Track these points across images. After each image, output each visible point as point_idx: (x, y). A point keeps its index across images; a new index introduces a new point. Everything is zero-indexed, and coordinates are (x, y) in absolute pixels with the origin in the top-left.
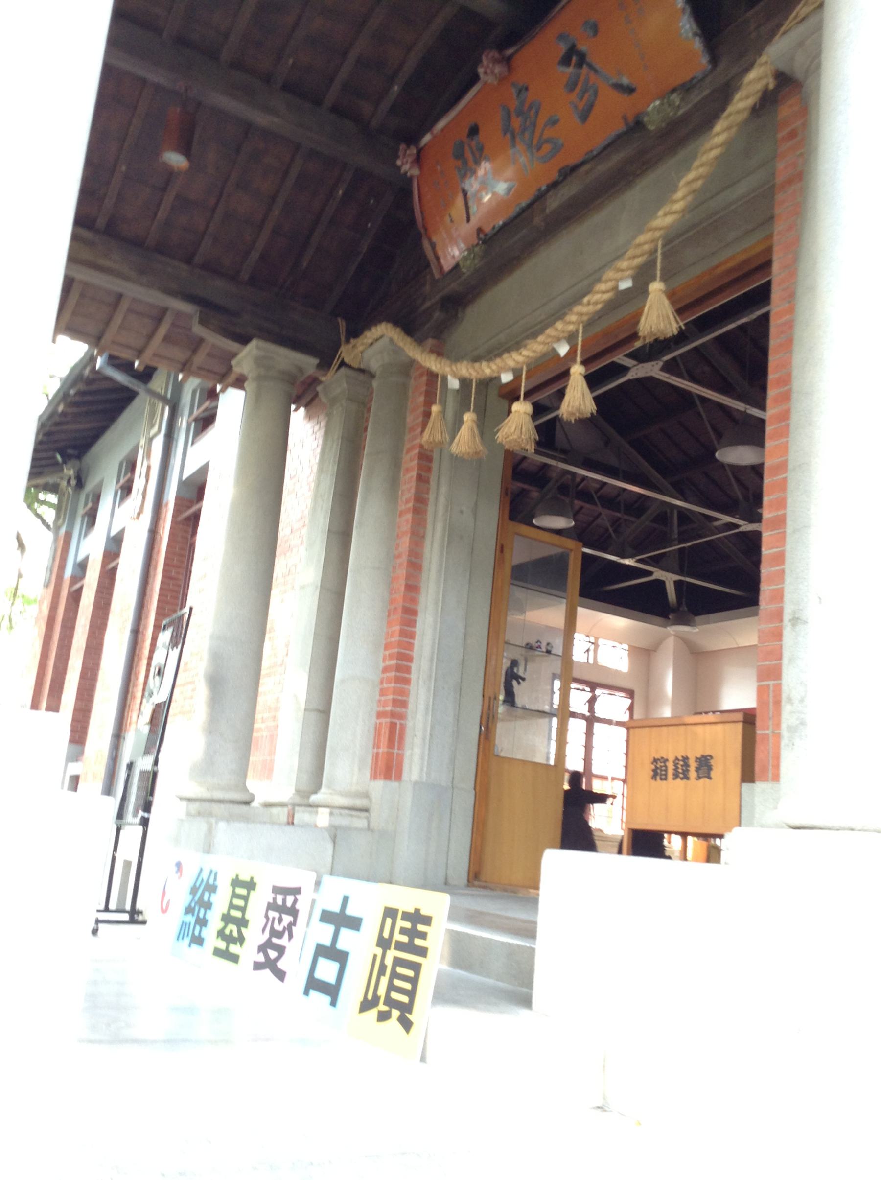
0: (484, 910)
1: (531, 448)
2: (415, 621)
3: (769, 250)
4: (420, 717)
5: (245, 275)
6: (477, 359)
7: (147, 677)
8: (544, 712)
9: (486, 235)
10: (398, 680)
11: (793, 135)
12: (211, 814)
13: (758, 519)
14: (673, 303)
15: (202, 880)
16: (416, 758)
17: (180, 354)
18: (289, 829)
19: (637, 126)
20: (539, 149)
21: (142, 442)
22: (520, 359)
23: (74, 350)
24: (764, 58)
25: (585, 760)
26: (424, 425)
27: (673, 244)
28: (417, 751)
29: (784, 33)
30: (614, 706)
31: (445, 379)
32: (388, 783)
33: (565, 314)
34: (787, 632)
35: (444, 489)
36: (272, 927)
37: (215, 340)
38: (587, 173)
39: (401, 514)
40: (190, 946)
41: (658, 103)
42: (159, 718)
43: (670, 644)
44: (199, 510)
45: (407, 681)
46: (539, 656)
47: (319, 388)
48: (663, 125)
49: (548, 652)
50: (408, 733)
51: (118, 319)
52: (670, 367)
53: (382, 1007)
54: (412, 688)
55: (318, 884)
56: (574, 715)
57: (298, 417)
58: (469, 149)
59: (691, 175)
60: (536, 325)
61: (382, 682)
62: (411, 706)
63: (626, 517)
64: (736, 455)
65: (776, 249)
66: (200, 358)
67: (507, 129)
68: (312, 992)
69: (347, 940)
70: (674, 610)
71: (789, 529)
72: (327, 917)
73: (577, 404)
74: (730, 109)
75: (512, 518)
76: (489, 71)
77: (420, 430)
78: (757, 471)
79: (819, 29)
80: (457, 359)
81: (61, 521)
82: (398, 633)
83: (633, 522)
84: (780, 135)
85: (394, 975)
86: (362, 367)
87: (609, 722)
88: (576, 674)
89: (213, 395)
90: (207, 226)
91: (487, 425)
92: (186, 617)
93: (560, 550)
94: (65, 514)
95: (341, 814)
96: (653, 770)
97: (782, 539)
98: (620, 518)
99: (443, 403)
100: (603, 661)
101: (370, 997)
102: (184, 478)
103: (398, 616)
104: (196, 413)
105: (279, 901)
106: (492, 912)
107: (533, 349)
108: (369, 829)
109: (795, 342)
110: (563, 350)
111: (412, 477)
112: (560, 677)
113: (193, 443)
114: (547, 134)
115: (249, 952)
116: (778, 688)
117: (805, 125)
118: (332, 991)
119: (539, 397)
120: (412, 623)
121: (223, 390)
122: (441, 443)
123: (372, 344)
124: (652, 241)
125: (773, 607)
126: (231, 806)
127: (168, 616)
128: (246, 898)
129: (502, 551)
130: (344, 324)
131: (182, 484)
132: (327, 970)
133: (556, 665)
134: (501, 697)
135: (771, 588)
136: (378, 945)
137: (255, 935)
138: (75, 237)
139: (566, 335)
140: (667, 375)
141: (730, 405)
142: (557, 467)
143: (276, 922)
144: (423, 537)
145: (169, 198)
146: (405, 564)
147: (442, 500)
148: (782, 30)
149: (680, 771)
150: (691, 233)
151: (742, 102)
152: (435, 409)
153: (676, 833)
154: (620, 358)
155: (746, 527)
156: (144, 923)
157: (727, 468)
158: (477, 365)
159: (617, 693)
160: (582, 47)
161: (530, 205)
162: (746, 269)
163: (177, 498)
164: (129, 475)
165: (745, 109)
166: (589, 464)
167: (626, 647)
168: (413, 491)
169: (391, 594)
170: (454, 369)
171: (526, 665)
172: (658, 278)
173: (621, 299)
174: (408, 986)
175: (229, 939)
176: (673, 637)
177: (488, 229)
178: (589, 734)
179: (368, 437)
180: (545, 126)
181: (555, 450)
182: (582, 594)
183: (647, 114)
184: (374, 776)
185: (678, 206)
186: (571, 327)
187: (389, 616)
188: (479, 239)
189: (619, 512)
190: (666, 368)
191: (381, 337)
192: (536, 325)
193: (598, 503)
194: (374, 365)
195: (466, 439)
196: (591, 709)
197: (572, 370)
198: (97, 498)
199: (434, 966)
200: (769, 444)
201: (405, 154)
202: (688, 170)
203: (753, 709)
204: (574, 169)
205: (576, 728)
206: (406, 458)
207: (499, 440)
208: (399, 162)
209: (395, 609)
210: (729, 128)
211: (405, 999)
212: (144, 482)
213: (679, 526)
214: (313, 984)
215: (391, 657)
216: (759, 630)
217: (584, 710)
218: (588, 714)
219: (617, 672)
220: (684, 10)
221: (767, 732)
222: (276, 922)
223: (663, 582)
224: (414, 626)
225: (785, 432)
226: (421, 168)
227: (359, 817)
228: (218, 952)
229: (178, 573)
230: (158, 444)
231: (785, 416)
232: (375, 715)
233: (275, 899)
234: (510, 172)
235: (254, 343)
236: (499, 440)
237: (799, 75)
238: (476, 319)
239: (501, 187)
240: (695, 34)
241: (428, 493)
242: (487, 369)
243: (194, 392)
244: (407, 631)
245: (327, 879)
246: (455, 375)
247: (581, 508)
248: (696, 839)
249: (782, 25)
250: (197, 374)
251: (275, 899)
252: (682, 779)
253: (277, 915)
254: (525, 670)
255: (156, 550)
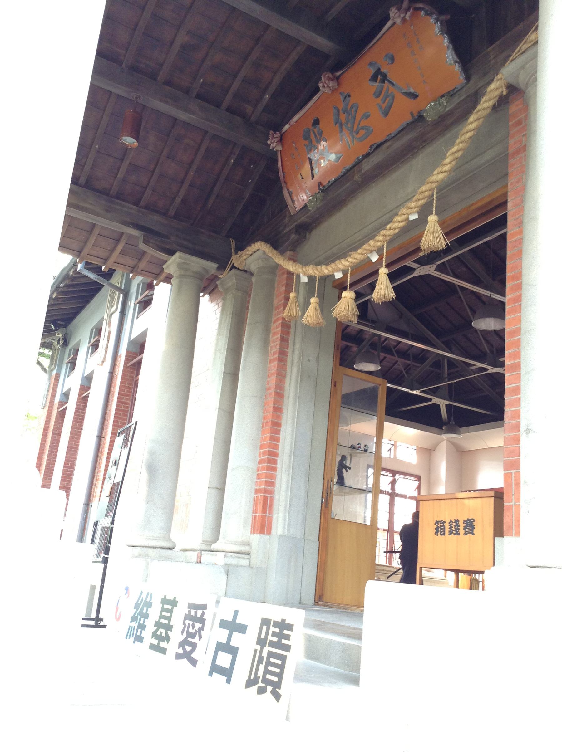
0: (326, 620)
1: (355, 320)
2: (280, 431)
3: (505, 194)
4: (283, 492)
5: (172, 212)
6: (318, 264)
7: (107, 466)
8: (363, 490)
9: (324, 187)
10: (269, 469)
11: (519, 123)
12: (147, 556)
13: (502, 365)
14: (442, 229)
15: (142, 600)
16: (281, 520)
17: (131, 262)
18: (199, 565)
19: (420, 118)
20: (357, 133)
21: (106, 316)
22: (347, 264)
23: (66, 259)
24: (499, 76)
25: (389, 521)
26: (285, 306)
27: (442, 192)
28: (281, 515)
29: (512, 61)
30: (407, 486)
31: (298, 277)
32: (262, 535)
33: (375, 236)
34: (524, 439)
35: (298, 346)
36: (188, 632)
37: (153, 253)
38: (388, 148)
39: (271, 362)
40: (134, 642)
41: (433, 104)
42: (115, 492)
43: (444, 446)
44: (141, 359)
45: (275, 469)
46: (360, 453)
47: (218, 282)
48: (436, 117)
49: (366, 451)
50: (276, 503)
51: (92, 240)
52: (440, 269)
53: (260, 684)
54: (278, 474)
55: (218, 602)
56: (382, 492)
57: (205, 300)
58: (313, 134)
59: (455, 149)
60: (355, 243)
61: (258, 470)
62: (277, 485)
63: (413, 363)
64: (486, 324)
65: (509, 194)
66: (143, 265)
67: (337, 121)
68: (214, 674)
69: (237, 640)
70: (446, 424)
71: (523, 372)
72: (224, 624)
73: (383, 293)
74: (479, 107)
75: (341, 365)
76: (325, 86)
77: (282, 308)
78: (500, 335)
79: (535, 57)
80: (305, 264)
81: (53, 366)
82: (268, 438)
83: (418, 367)
84: (511, 123)
85: (269, 663)
86: (245, 269)
87: (405, 497)
88: (384, 465)
89: (151, 287)
90: (148, 183)
91: (326, 306)
92: (133, 428)
93: (373, 385)
94: (56, 363)
95: (231, 556)
96: (436, 529)
97: (518, 377)
98: (409, 365)
99: (297, 292)
100: (399, 457)
101: (252, 677)
102: (132, 337)
103: (268, 427)
104: (140, 298)
105: (193, 613)
106: (330, 622)
107: (355, 257)
108: (250, 566)
109: (524, 252)
110: (374, 258)
111: (277, 338)
112: (373, 467)
113: (137, 318)
114: (362, 124)
115: (173, 647)
116: (518, 475)
117: (527, 117)
118: (227, 673)
119: (358, 287)
120: (278, 432)
121: (157, 284)
122: (296, 317)
123: (251, 255)
124: (430, 190)
125: (513, 422)
126: (160, 550)
127: (122, 427)
128: (171, 611)
129: (335, 386)
130: (234, 242)
131: (131, 343)
132: (224, 660)
133: (371, 460)
134: (335, 480)
135: (511, 409)
136: (257, 643)
137: (177, 636)
138: (71, 191)
139: (376, 248)
140: (439, 273)
141: (480, 292)
142: (369, 332)
143: (191, 627)
144: (285, 376)
145: (125, 166)
146: (273, 394)
147: (297, 353)
148: (511, 58)
149: (453, 529)
150: (454, 185)
151: (486, 103)
152: (292, 295)
153: (464, 572)
154: (409, 263)
155: (492, 370)
156: (104, 627)
157: (479, 332)
158: (319, 267)
159: (410, 478)
160: (384, 70)
161: (352, 168)
162: (490, 207)
163: (127, 352)
164: (97, 337)
165: (488, 107)
166: (390, 330)
167: (415, 448)
168: (278, 347)
169: (264, 413)
170: (304, 270)
171: (351, 459)
172: (434, 213)
173: (410, 226)
174: (278, 671)
175: (160, 638)
176: (445, 442)
177: (325, 183)
178: (392, 504)
179: (249, 313)
180: (361, 119)
181: (368, 320)
182: (387, 414)
183: (426, 110)
184: (253, 531)
185: (446, 168)
186: (379, 244)
187: (263, 427)
188: (320, 189)
189: (409, 360)
190: (438, 269)
191: (258, 250)
192: (355, 243)
193: (395, 354)
194: (253, 268)
195: (312, 314)
196: (393, 488)
197: (380, 271)
198: (76, 352)
199: (296, 657)
200: (507, 317)
201: (272, 138)
202: (453, 145)
203: (502, 488)
204: (379, 146)
205: (384, 500)
206: (273, 326)
207: (334, 316)
208: (269, 142)
209: (267, 422)
210: (478, 119)
211: (276, 679)
212: (107, 342)
213: (448, 370)
214: (215, 669)
215: (264, 453)
216: (504, 437)
217: (388, 488)
218: (390, 491)
219: (409, 464)
220: (448, 47)
221: (511, 504)
222: (191, 627)
223: (438, 406)
224: (279, 434)
225: (518, 309)
226: (283, 146)
227: (243, 558)
228: (152, 647)
229: (127, 399)
230: (116, 317)
231: (518, 299)
232: (253, 492)
233: (190, 612)
234: (338, 147)
235: (177, 254)
236: (334, 316)
237: (522, 87)
238: (317, 239)
239: (332, 157)
240: (456, 62)
241: (287, 349)
242: (325, 270)
243: (139, 285)
244: (275, 437)
245: (223, 600)
246: (305, 274)
247: (385, 357)
248: (462, 574)
249: (511, 56)
250: (140, 274)
251: (190, 612)
252: (455, 534)
253: (191, 623)
254: (351, 463)
255: (113, 385)
